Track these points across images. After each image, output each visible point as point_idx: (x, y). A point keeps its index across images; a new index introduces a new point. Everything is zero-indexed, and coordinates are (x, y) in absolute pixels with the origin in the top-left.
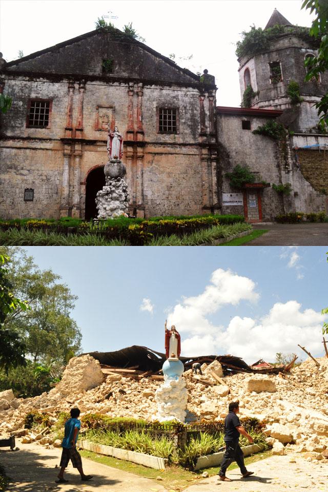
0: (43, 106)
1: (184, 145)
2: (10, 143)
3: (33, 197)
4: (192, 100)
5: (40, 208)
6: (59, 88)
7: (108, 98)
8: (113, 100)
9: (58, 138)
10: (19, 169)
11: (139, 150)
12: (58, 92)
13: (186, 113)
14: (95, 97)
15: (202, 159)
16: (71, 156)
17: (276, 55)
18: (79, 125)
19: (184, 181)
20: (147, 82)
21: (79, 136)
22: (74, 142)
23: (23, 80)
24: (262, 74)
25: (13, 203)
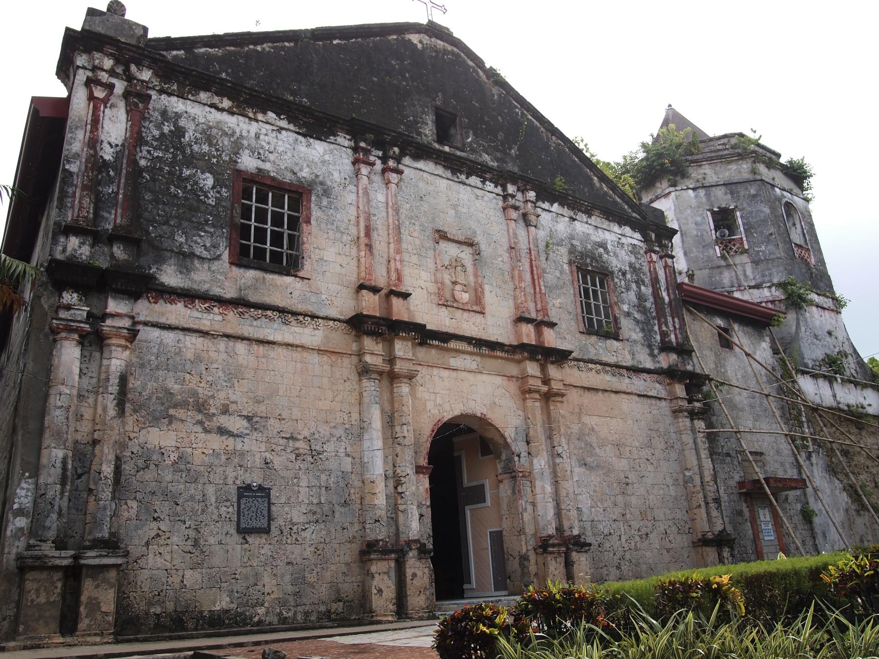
0: (262, 199)
1: (636, 370)
2: (177, 312)
3: (270, 518)
4: (633, 260)
5: (295, 557)
6: (327, 157)
7: (458, 215)
8: (474, 225)
9: (333, 313)
10: (213, 410)
11: (553, 371)
13: (628, 289)
14: (425, 207)
15: (676, 412)
17: (726, 194)
19: (651, 468)
20: (547, 194)
22: (379, 327)
23: (213, 106)
24: (695, 233)
25: (196, 543)
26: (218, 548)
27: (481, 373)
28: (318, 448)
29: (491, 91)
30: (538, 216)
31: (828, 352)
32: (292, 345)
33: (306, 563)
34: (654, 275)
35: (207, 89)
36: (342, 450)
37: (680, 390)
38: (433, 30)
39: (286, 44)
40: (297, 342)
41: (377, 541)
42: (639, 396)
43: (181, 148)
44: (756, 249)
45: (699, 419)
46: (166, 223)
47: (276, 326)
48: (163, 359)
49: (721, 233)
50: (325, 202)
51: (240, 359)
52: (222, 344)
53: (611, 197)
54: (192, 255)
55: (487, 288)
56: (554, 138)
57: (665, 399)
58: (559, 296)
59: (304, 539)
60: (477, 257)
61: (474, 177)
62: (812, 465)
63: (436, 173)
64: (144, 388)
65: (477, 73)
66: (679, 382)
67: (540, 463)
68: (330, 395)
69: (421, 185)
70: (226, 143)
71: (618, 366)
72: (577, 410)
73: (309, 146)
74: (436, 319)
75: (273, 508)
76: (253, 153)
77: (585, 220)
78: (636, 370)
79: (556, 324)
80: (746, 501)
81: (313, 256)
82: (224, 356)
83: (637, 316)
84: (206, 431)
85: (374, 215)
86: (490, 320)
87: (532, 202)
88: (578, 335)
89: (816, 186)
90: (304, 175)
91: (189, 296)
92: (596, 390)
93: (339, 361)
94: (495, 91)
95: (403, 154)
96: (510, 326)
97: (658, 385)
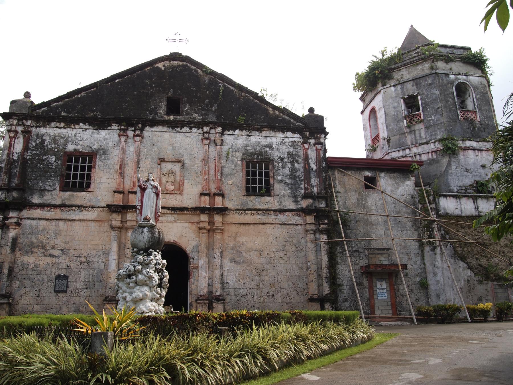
2: (37, 213)
3: (67, 287)
6: (107, 137)
7: (173, 148)
8: (182, 152)
10: (48, 248)
11: (218, 218)
13: (284, 167)
14: (156, 148)
15: (307, 231)
17: (413, 86)
20: (229, 126)
23: (57, 127)
24: (393, 113)
25: (39, 296)
26: (46, 297)
28: (90, 260)
29: (204, 78)
31: (478, 179)
32: (82, 220)
33: (81, 303)
35: (54, 121)
36: (101, 260)
38: (175, 56)
39: (92, 90)
40: (85, 218)
41: (108, 296)
42: (280, 224)
43: (43, 148)
44: (429, 119)
45: (323, 234)
46: (36, 179)
47: (76, 213)
48: (31, 231)
50: (103, 157)
51: (61, 228)
52: (54, 223)
53: (281, 117)
54: (45, 190)
55: (186, 181)
57: (301, 225)
58: (232, 178)
59: (81, 295)
60: (182, 167)
62: (435, 254)
64: (23, 242)
65: (197, 71)
68: (97, 238)
69: (154, 138)
70: (62, 141)
71: (267, 210)
72: (234, 235)
73: (98, 133)
75: (69, 283)
76: (73, 143)
78: (282, 211)
80: (366, 277)
81: (95, 182)
82: (54, 227)
83: (288, 181)
84: (45, 256)
85: (127, 158)
86: (185, 196)
87: (220, 133)
88: (242, 197)
89: (493, 65)
90: (95, 147)
91: (42, 206)
92: (249, 224)
94: (207, 78)
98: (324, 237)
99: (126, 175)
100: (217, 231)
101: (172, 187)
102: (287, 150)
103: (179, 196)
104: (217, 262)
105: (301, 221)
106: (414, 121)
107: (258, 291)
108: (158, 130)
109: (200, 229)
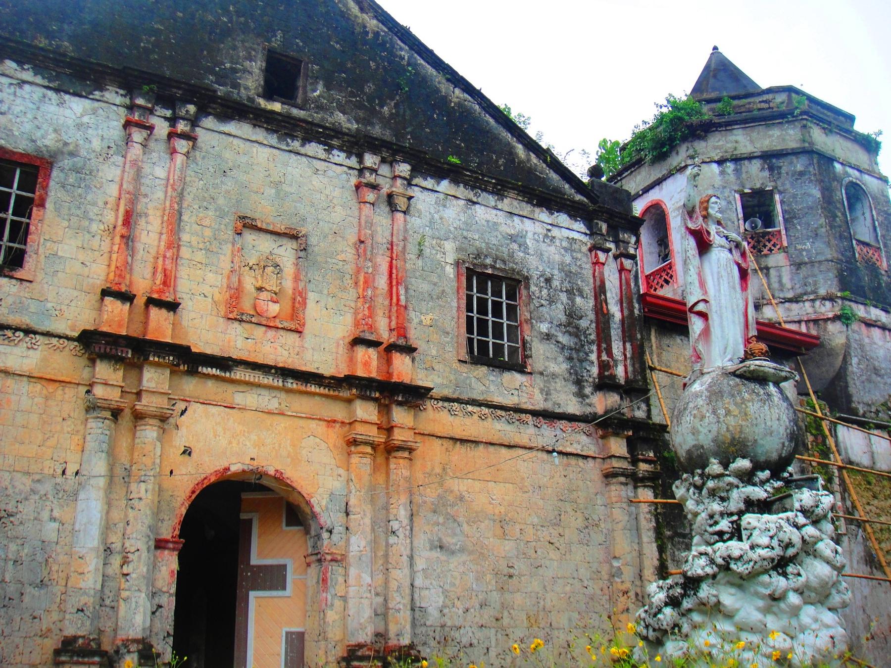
4: (568, 259)
6: (86, 119)
7: (280, 196)
11: (400, 416)
12: (79, 135)
13: (551, 301)
14: (229, 185)
15: (609, 476)
16: (122, 415)
17: (763, 169)
18: (165, 283)
19: (554, 555)
20: (429, 166)
21: (160, 327)
22: (131, 349)
27: (283, 414)
30: (410, 198)
34: (598, 283)
37: (618, 446)
41: (75, 638)
44: (799, 247)
45: (645, 486)
49: (752, 222)
55: (312, 297)
56: (457, 91)
57: (594, 458)
60: (302, 254)
61: (313, 144)
63: (254, 138)
66: (616, 434)
67: (358, 544)
69: (227, 155)
71: (518, 410)
72: (438, 470)
73: (61, 104)
74: (234, 341)
77: (493, 204)
79: (415, 349)
81: (41, 251)
83: (564, 339)
85: (146, 196)
87: (404, 178)
93: (60, 392)
95: (203, 111)
96: (342, 350)
97: (584, 437)
98: (646, 494)
99: (139, 246)
100: (399, 454)
101: (274, 309)
102: (557, 258)
103: (291, 339)
104: (400, 544)
105: (593, 448)
106: (765, 246)
107: (499, 636)
108: (238, 133)
109: (354, 442)
